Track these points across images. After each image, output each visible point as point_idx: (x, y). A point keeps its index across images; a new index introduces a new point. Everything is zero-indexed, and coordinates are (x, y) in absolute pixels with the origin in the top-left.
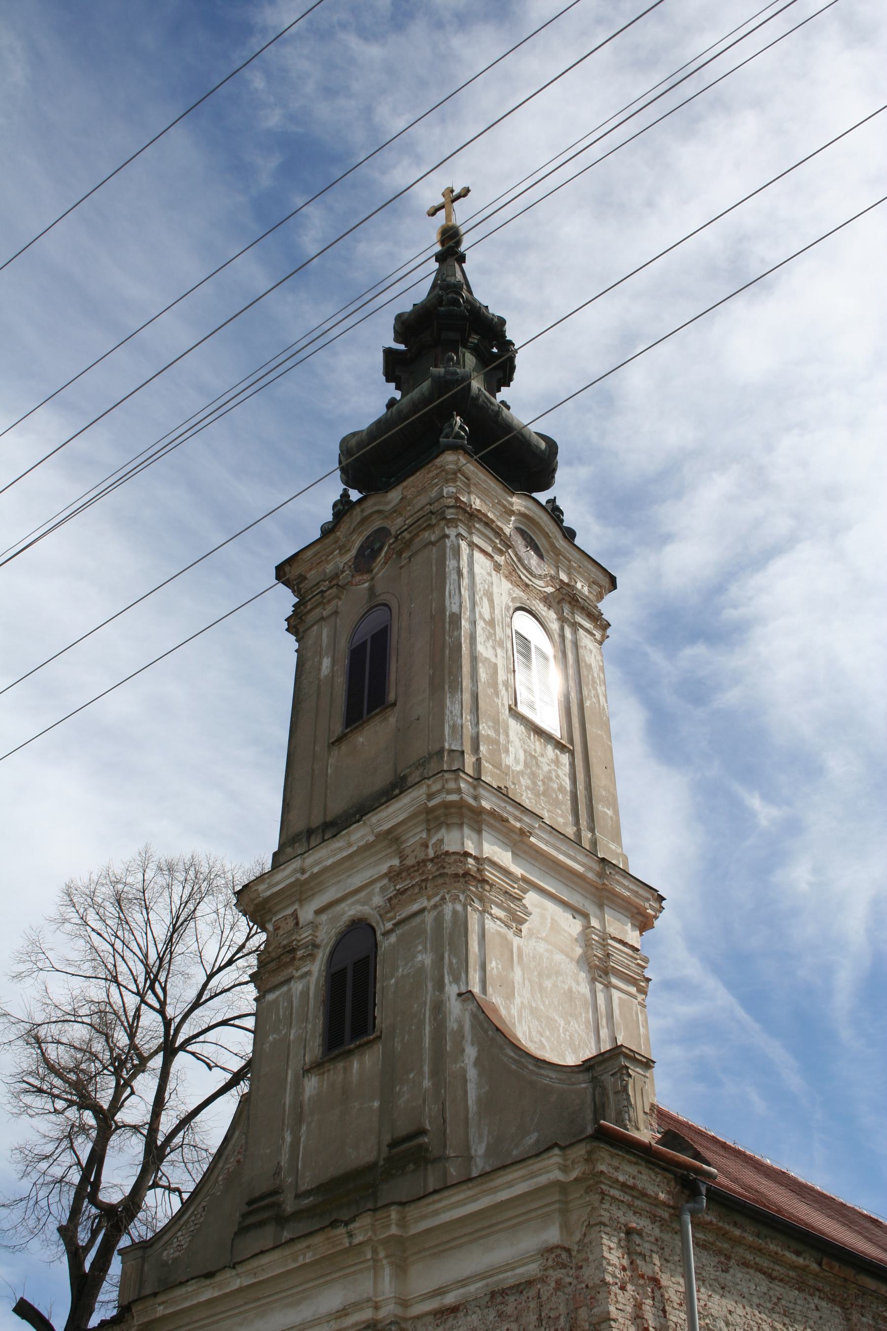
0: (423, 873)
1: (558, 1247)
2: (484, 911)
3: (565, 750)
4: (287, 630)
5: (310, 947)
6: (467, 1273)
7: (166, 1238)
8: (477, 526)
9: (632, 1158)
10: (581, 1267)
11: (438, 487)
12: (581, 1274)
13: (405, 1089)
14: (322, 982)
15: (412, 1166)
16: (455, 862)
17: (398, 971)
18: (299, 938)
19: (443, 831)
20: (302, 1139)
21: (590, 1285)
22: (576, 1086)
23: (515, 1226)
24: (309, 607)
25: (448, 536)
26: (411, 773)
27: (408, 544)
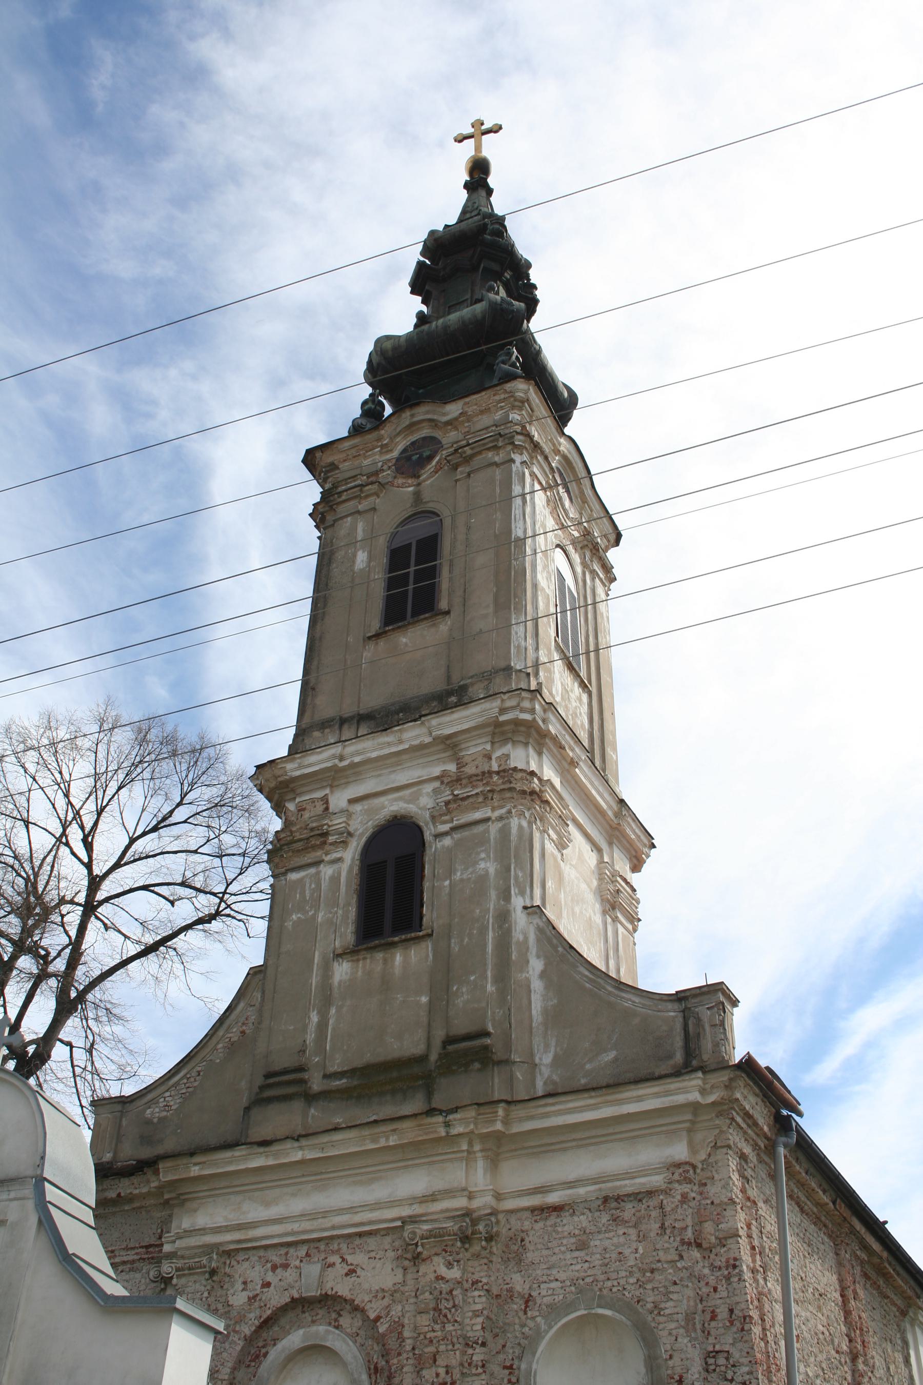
0: (487, 784)
1: (686, 1163)
2: (544, 831)
3: (586, 690)
4: (310, 515)
5: (345, 835)
6: (572, 1177)
7: (150, 1096)
8: (539, 458)
9: (757, 1091)
10: (705, 1184)
11: (504, 411)
12: (705, 1191)
13: (464, 990)
14: (356, 870)
15: (477, 1065)
16: (522, 779)
17: (455, 874)
18: (330, 823)
19: (509, 746)
20: (331, 1022)
21: (716, 1202)
22: (666, 1014)
23: (634, 1137)
24: (344, 498)
25: (513, 461)
26: (472, 684)
27: (467, 460)
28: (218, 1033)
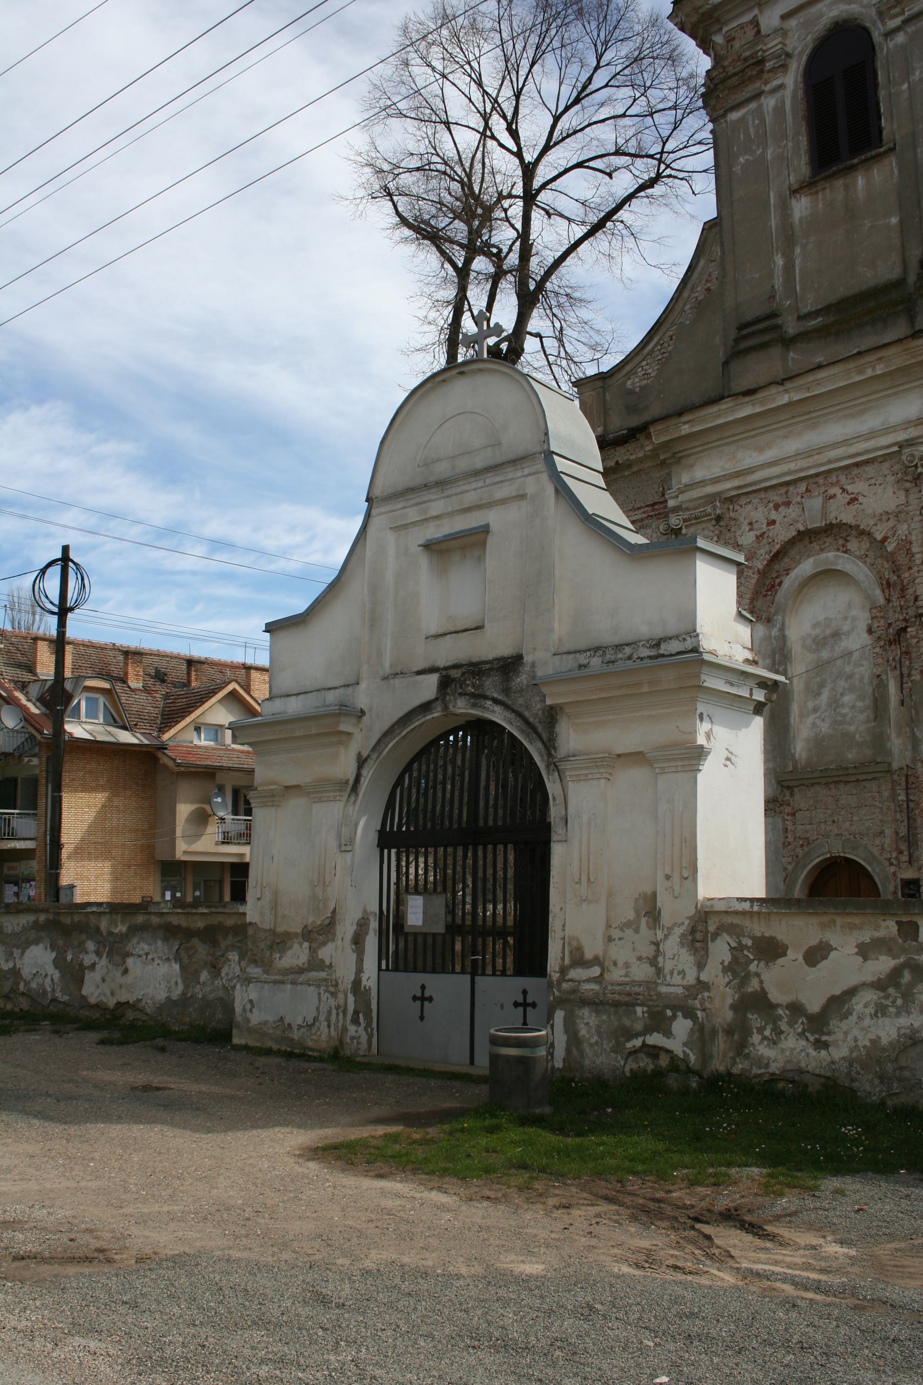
7: (628, 368)
14: (800, 94)
17: (913, 74)
18: (765, 48)
20: (797, 262)
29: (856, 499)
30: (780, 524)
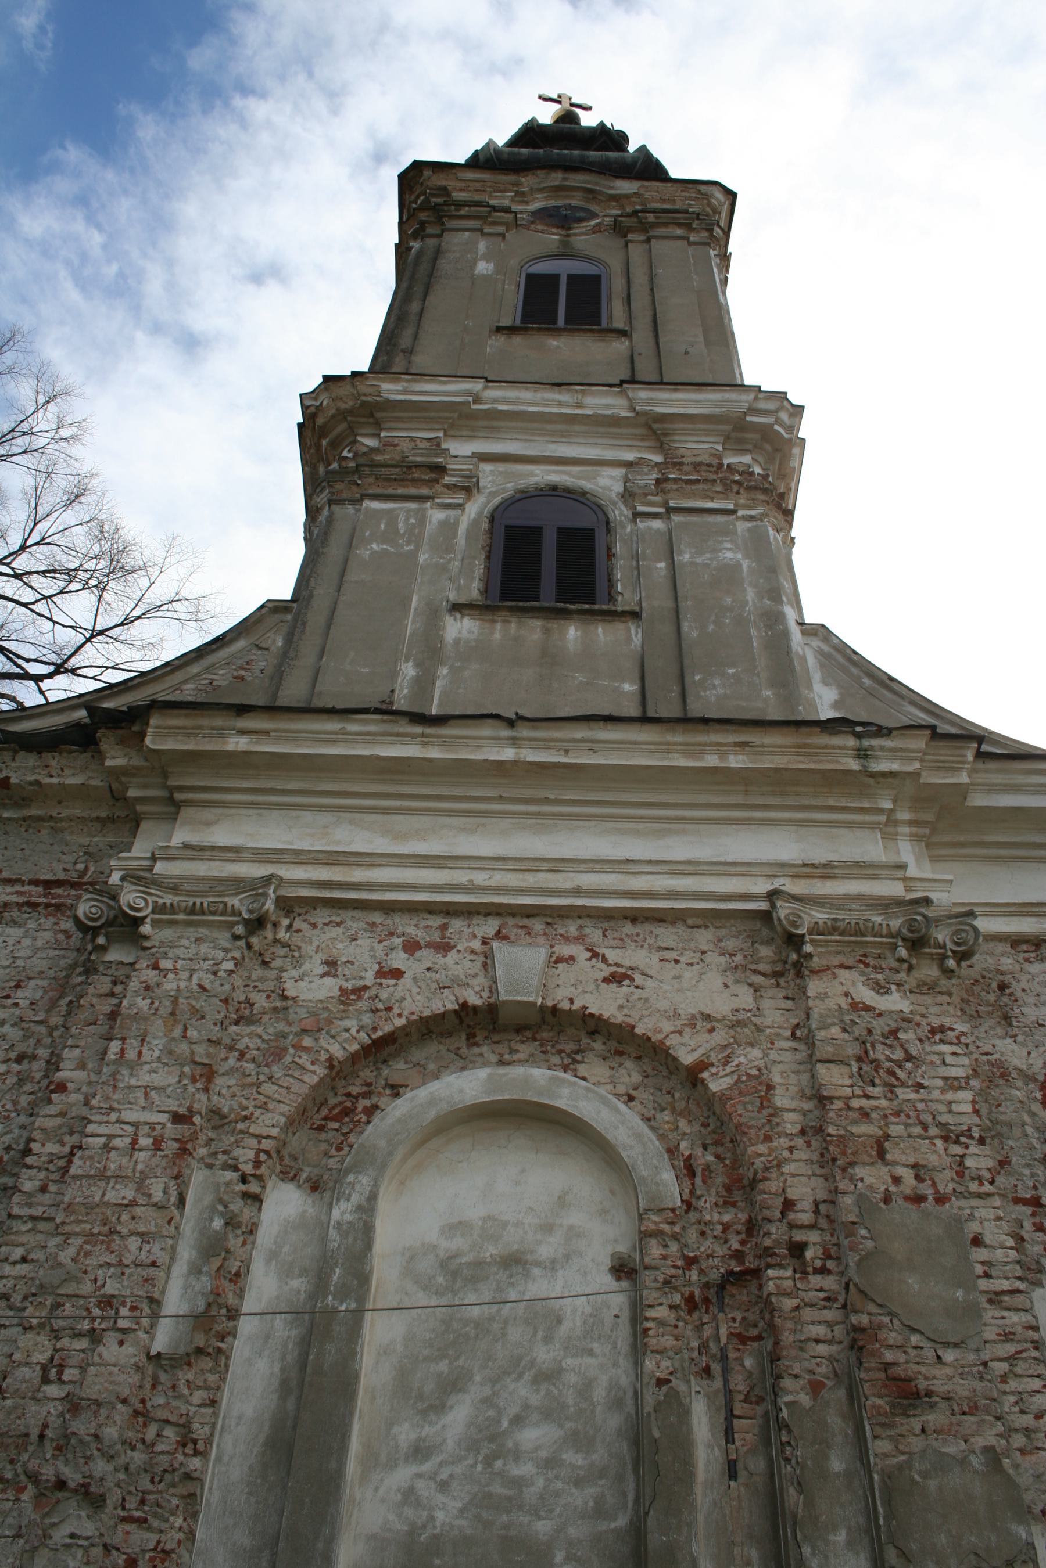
28: (188, 668)
29: (625, 976)
30: (415, 979)
